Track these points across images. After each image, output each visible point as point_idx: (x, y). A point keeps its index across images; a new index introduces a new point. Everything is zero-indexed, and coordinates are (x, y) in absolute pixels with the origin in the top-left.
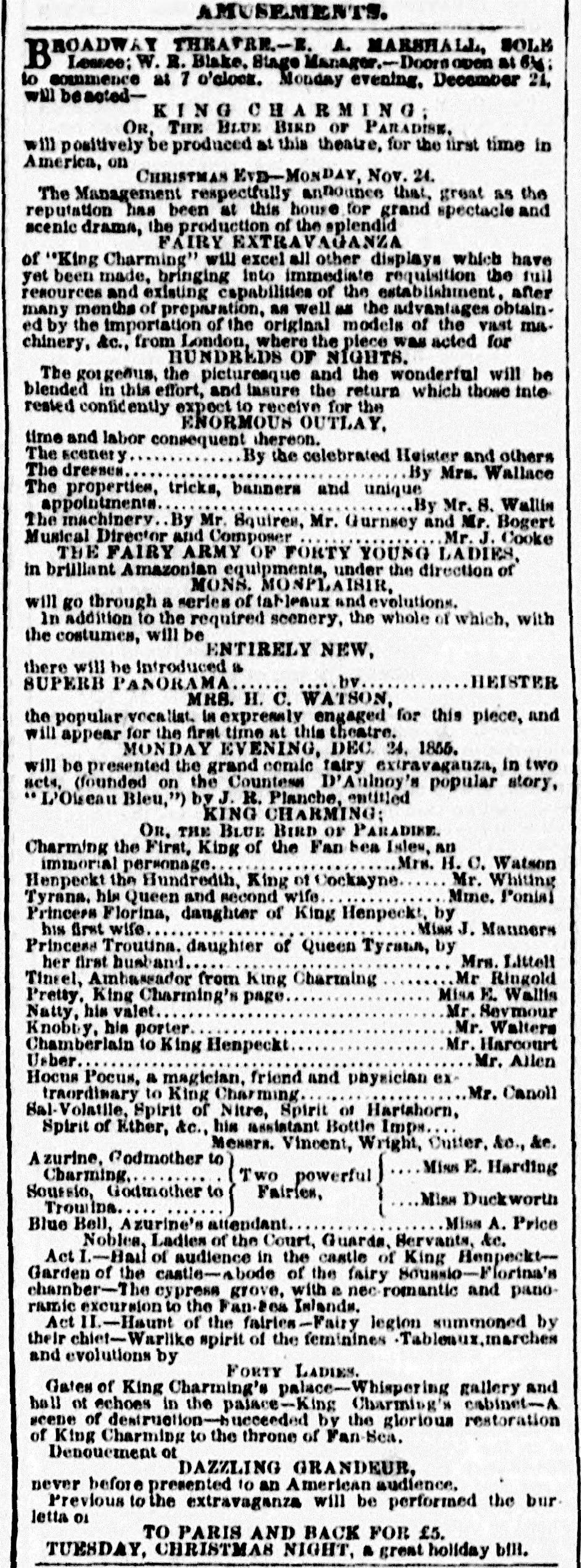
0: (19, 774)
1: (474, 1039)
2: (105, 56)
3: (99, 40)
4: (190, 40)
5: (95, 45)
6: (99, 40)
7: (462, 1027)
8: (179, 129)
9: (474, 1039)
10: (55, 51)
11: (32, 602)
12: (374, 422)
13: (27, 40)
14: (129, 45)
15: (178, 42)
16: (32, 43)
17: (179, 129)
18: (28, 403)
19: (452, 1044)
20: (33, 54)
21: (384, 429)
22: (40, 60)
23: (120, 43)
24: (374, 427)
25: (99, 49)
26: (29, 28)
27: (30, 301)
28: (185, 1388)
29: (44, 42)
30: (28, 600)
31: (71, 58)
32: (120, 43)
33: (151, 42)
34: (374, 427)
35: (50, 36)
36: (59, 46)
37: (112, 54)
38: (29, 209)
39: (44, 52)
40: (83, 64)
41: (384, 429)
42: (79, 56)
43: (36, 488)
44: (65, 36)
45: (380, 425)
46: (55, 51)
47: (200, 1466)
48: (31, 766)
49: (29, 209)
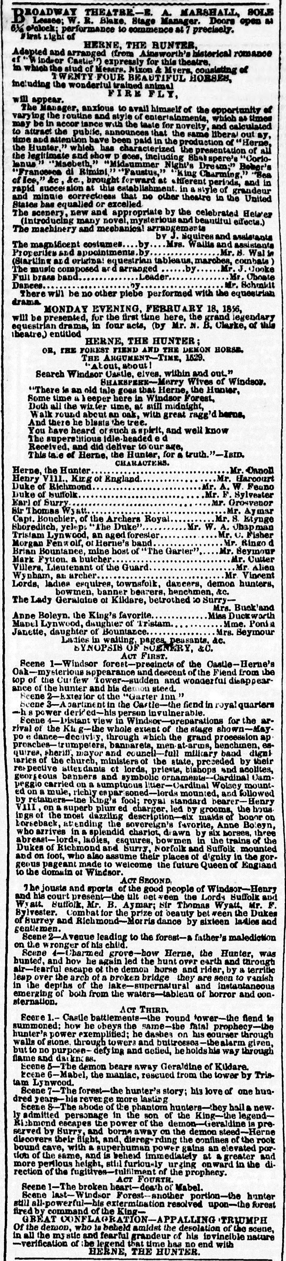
0: (9, 322)
1: (233, 549)
2: (51, 17)
4: (93, 10)
5: (46, 12)
7: (227, 543)
8: (145, 1010)
9: (233, 549)
11: (16, 100)
12: (171, 94)
15: (88, 11)
16: (15, 10)
17: (145, 1010)
18: (16, 1171)
19: (223, 551)
20: (16, 16)
21: (177, 97)
22: (19, 19)
23: (58, 12)
24: (171, 96)
25: (48, 14)
26: (14, 3)
27: (18, 1038)
28: (105, 1172)
29: (22, 10)
30: (13, 81)
31: (35, 18)
32: (58, 12)
33: (74, 11)
34: (171, 96)
35: (24, 7)
36: (28, 12)
37: (54, 16)
38: (14, 727)
39: (21, 15)
40: (41, 21)
41: (177, 97)
42: (39, 17)
43: (18, 213)
44: (32, 7)
45: (174, 95)
46: (26, 14)
47: (78, 308)
48: (15, 318)
49: (14, 727)
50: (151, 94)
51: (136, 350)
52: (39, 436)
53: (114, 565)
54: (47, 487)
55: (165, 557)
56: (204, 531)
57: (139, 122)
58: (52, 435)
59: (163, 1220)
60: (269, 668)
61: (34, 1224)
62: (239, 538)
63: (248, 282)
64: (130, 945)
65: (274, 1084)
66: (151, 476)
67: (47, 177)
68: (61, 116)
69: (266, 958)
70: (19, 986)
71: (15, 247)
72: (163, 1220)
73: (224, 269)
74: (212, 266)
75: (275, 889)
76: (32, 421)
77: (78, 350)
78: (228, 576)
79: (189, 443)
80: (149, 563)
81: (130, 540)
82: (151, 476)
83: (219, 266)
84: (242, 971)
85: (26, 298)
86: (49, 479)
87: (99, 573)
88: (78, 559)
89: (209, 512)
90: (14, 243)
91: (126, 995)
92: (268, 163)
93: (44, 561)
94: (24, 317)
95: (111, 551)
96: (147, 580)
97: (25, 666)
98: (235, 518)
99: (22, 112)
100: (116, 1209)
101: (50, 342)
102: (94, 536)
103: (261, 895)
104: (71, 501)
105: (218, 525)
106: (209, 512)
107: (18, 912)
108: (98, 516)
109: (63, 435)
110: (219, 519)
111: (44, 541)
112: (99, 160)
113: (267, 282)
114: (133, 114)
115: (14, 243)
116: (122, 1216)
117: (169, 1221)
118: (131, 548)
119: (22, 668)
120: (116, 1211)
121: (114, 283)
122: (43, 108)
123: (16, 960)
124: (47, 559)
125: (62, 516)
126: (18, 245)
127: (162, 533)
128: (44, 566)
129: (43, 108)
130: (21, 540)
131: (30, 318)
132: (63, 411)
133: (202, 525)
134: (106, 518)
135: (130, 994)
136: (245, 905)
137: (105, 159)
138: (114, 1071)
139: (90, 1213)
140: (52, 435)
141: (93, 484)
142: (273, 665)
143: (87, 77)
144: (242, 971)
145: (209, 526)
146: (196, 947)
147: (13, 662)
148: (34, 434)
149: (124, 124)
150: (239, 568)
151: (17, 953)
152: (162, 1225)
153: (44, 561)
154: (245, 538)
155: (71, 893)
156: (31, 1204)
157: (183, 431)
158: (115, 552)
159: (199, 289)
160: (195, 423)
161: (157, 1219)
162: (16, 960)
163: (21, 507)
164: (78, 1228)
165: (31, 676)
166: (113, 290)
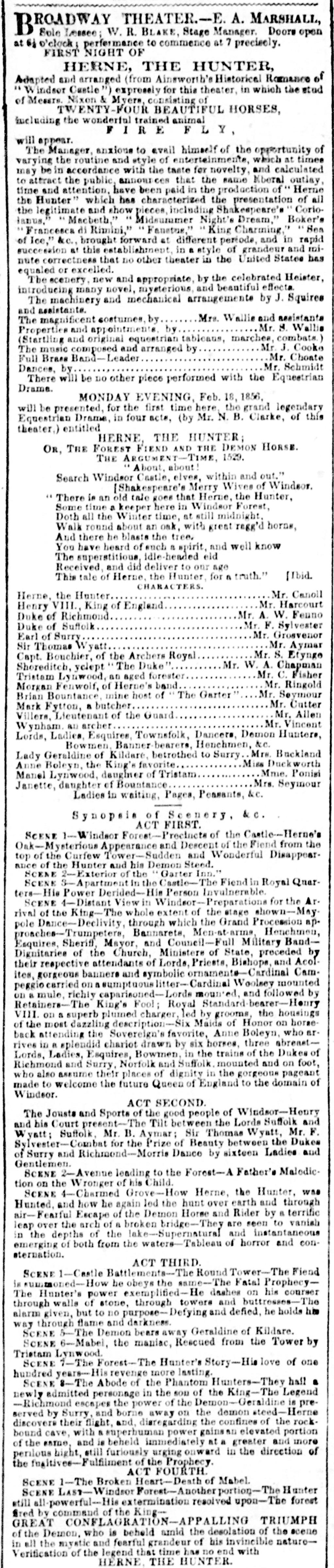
10: (37, 23)
13: (15, 13)
14: (91, 19)
16: (19, 16)
35: (32, 11)
44: (45, 11)
50: (141, 131)
51: (165, 448)
52: (69, 553)
53: (135, 712)
54: (59, 616)
55: (197, 701)
56: (243, 670)
57: (165, 166)
58: (83, 553)
59: (187, 1521)
60: (315, 840)
61: (33, 1530)
62: (280, 677)
63: (292, 363)
64: (179, 1183)
65: (319, 1353)
66: (177, 603)
67: (56, 237)
68: (73, 161)
69: (310, 1197)
70: (20, 1236)
72: (187, 1521)
73: (265, 348)
74: (248, 344)
75: (317, 1111)
76: (59, 536)
77: (90, 448)
78: (269, 723)
79: (235, 561)
80: (174, 710)
81: (153, 682)
82: (177, 603)
83: (258, 345)
84: (282, 1214)
85: (35, 385)
86: (59, 606)
87: (115, 722)
88: (93, 706)
89: (247, 646)
91: (140, 1245)
92: (321, 215)
93: (52, 708)
94: (31, 408)
95: (131, 695)
96: (174, 731)
97: (30, 840)
98: (277, 654)
99: (27, 157)
100: (132, 1509)
101: (51, 439)
102: (111, 677)
103: (300, 1119)
104: (85, 634)
105: (260, 663)
106: (247, 646)
107: (17, 1144)
108: (119, 653)
109: (93, 553)
110: (259, 654)
111: (53, 684)
112: (119, 215)
113: (315, 363)
114: (158, 156)
116: (138, 1518)
117: (194, 1523)
118: (154, 691)
119: (27, 842)
120: (132, 1512)
121: (159, 365)
122: (52, 150)
123: (18, 1204)
124: (55, 707)
125: (75, 653)
127: (187, 673)
128: (52, 715)
129: (52, 150)
130: (29, 682)
131: (38, 408)
132: (96, 522)
133: (241, 664)
134: (127, 654)
135: (145, 1244)
136: (284, 1131)
137: (126, 214)
138: (199, 1337)
139: (101, 1515)
140: (83, 553)
141: (112, 612)
142: (319, 835)
143: (103, 110)
144: (282, 1214)
145: (250, 665)
146: (230, 1183)
147: (16, 835)
148: (62, 551)
149: (147, 171)
150: (279, 714)
151: (18, 1193)
152: (187, 1529)
153: (52, 708)
154: (290, 678)
155: (81, 1120)
156: (32, 1504)
157: (229, 547)
158: (135, 696)
159: (225, 374)
160: (242, 537)
161: (180, 1520)
162: (18, 1204)
163: (28, 642)
164: (87, 1533)
165: (38, 851)
166: (158, 374)
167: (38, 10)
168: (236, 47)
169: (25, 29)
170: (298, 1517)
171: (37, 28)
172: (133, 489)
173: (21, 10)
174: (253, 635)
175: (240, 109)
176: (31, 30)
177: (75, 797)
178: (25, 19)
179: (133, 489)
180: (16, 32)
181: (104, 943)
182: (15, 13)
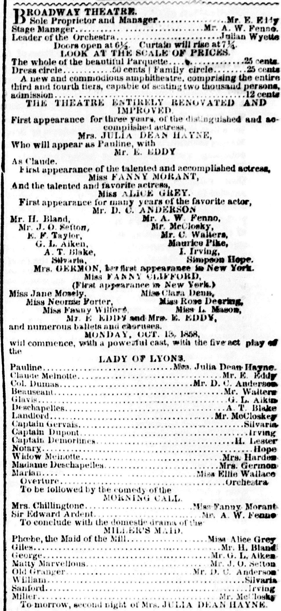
3: (50, 10)
6: (50, 10)
10: (28, 15)
13: (14, 9)
14: (66, 12)
16: (16, 11)
35: (25, 8)
44: (34, 8)
71: (14, 64)
90: (14, 60)
115: (14, 60)
126: (17, 62)
150: (225, 547)
167: (29, 7)
168: (174, 166)
169: (20, 20)
170: (260, 607)
171: (28, 18)
172: (30, 71)
173: (17, 7)
174: (173, 367)
175: (163, 119)
176: (24, 20)
177: (101, 361)
178: (20, 13)
179: (30, 71)
180: (14, 21)
181: (67, 318)
182: (14, 9)
